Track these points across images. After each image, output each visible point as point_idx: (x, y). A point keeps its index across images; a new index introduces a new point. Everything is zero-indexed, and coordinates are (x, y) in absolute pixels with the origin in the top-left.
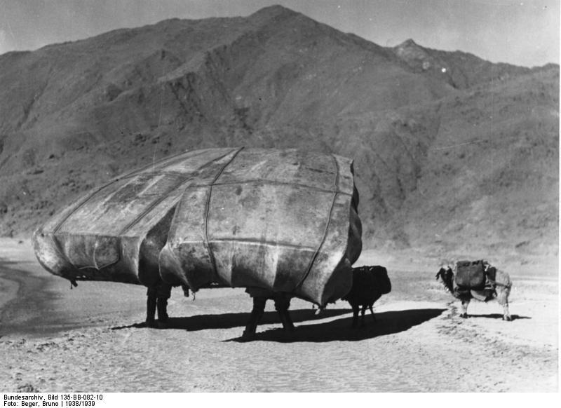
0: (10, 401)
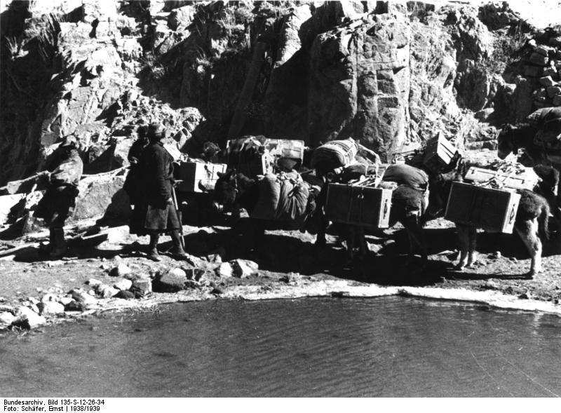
0: (10, 406)
